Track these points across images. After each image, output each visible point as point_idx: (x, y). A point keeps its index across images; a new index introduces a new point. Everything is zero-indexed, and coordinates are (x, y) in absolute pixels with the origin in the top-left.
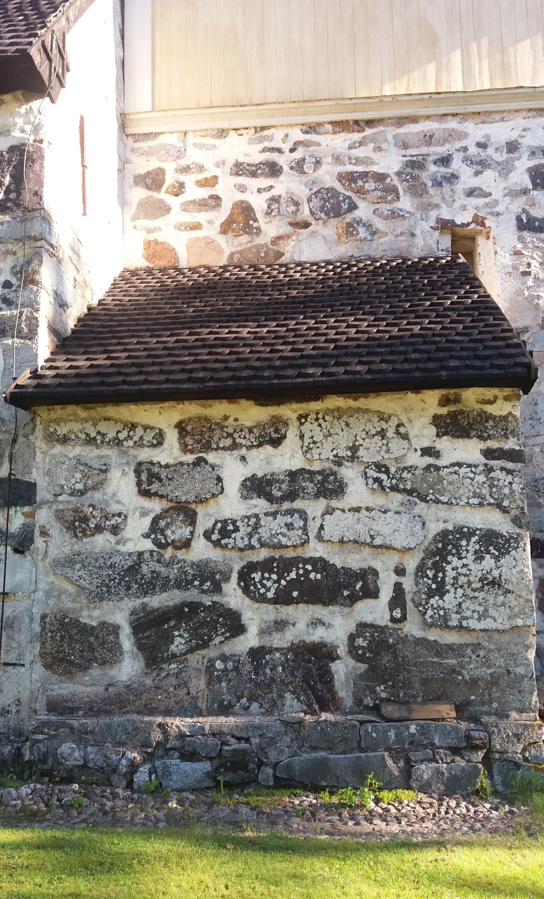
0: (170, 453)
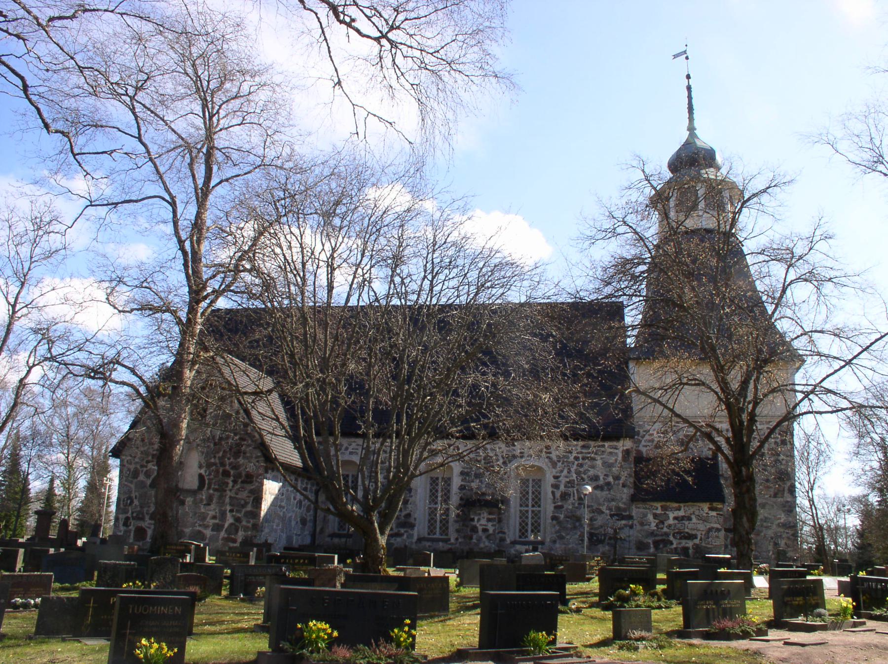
0: (659, 511)
